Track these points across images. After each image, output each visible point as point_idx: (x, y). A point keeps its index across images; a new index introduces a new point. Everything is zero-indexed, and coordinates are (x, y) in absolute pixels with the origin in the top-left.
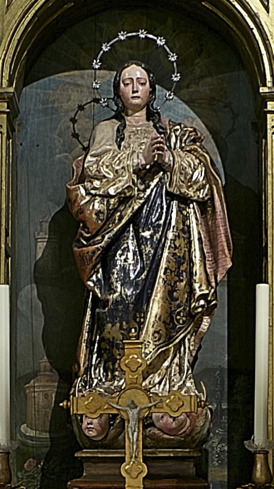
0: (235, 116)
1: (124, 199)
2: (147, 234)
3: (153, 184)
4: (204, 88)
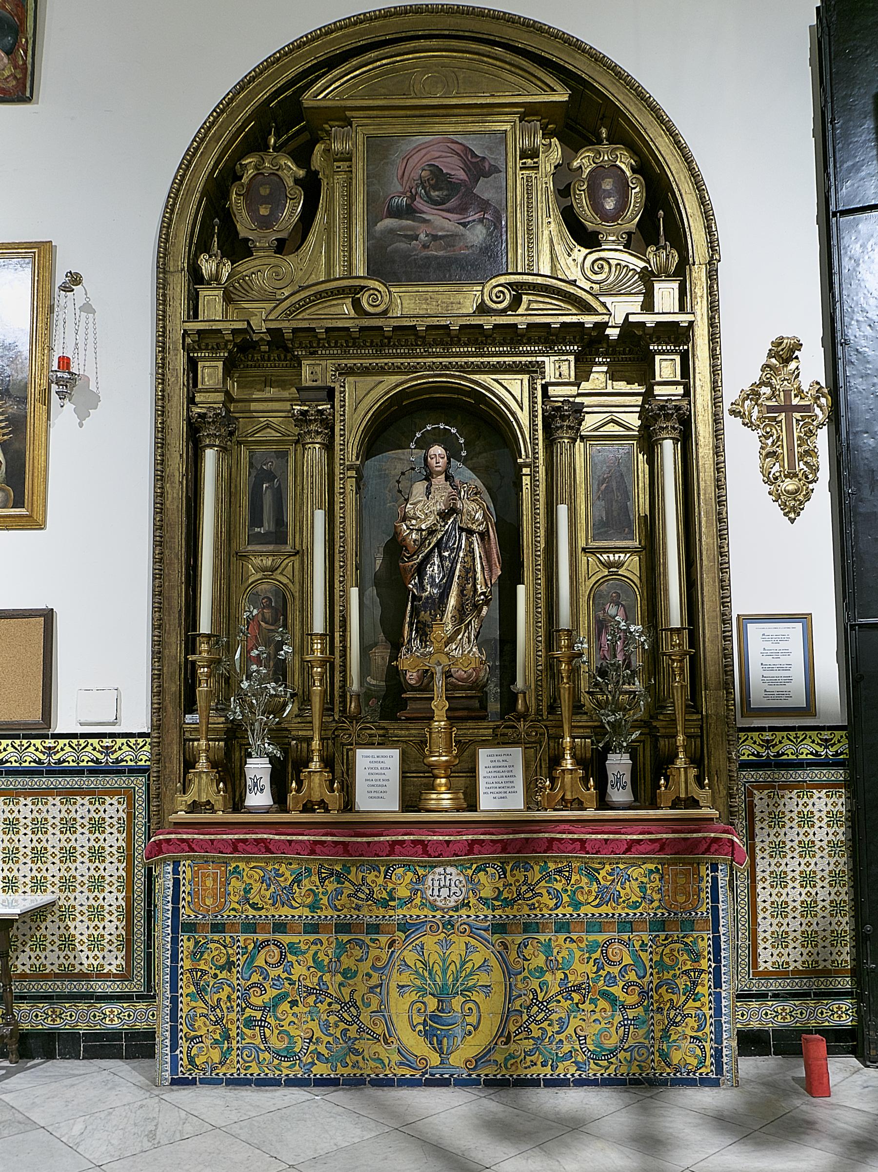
0: (502, 478)
1: (431, 532)
2: (446, 554)
3: (450, 522)
4: (482, 460)
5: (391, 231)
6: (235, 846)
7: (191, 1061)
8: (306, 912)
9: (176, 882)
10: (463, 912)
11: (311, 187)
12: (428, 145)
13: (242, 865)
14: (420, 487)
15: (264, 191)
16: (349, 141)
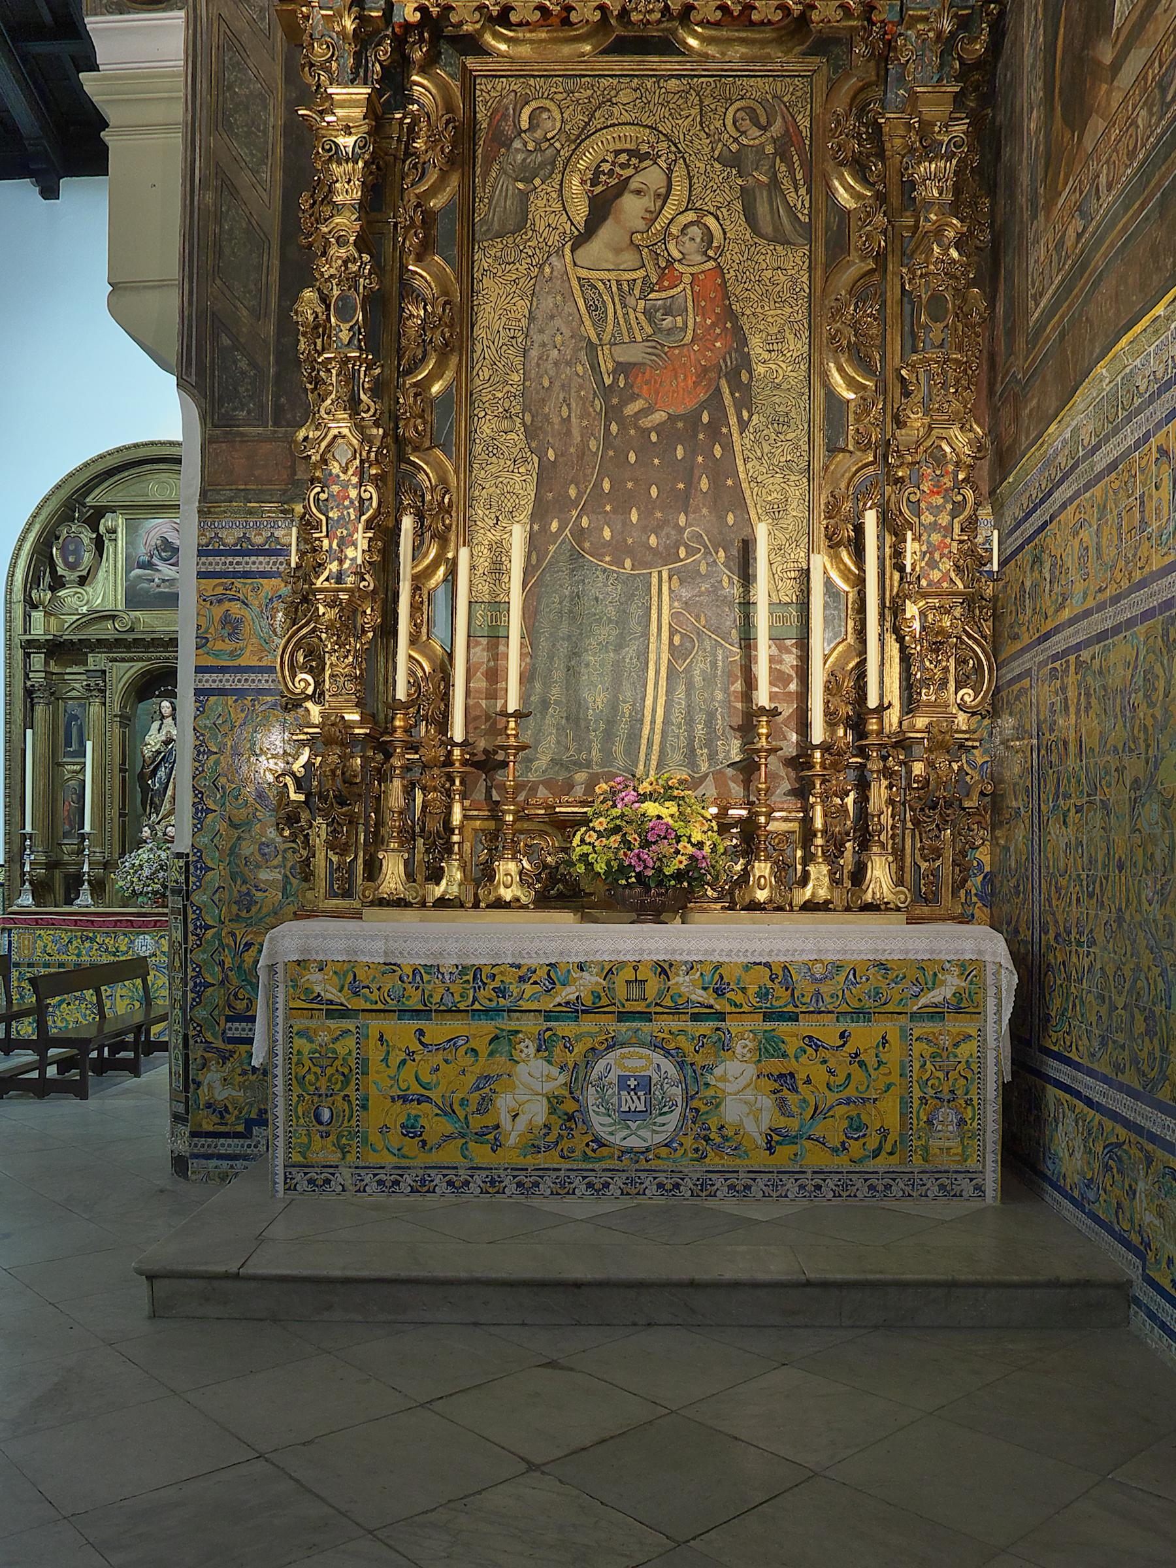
5: (139, 577)
6: (37, 921)
7: (18, 1033)
8: (75, 958)
9: (10, 942)
10: (153, 958)
11: (99, 544)
12: (161, 524)
13: (42, 932)
14: (156, 725)
15: (71, 547)
16: (116, 521)
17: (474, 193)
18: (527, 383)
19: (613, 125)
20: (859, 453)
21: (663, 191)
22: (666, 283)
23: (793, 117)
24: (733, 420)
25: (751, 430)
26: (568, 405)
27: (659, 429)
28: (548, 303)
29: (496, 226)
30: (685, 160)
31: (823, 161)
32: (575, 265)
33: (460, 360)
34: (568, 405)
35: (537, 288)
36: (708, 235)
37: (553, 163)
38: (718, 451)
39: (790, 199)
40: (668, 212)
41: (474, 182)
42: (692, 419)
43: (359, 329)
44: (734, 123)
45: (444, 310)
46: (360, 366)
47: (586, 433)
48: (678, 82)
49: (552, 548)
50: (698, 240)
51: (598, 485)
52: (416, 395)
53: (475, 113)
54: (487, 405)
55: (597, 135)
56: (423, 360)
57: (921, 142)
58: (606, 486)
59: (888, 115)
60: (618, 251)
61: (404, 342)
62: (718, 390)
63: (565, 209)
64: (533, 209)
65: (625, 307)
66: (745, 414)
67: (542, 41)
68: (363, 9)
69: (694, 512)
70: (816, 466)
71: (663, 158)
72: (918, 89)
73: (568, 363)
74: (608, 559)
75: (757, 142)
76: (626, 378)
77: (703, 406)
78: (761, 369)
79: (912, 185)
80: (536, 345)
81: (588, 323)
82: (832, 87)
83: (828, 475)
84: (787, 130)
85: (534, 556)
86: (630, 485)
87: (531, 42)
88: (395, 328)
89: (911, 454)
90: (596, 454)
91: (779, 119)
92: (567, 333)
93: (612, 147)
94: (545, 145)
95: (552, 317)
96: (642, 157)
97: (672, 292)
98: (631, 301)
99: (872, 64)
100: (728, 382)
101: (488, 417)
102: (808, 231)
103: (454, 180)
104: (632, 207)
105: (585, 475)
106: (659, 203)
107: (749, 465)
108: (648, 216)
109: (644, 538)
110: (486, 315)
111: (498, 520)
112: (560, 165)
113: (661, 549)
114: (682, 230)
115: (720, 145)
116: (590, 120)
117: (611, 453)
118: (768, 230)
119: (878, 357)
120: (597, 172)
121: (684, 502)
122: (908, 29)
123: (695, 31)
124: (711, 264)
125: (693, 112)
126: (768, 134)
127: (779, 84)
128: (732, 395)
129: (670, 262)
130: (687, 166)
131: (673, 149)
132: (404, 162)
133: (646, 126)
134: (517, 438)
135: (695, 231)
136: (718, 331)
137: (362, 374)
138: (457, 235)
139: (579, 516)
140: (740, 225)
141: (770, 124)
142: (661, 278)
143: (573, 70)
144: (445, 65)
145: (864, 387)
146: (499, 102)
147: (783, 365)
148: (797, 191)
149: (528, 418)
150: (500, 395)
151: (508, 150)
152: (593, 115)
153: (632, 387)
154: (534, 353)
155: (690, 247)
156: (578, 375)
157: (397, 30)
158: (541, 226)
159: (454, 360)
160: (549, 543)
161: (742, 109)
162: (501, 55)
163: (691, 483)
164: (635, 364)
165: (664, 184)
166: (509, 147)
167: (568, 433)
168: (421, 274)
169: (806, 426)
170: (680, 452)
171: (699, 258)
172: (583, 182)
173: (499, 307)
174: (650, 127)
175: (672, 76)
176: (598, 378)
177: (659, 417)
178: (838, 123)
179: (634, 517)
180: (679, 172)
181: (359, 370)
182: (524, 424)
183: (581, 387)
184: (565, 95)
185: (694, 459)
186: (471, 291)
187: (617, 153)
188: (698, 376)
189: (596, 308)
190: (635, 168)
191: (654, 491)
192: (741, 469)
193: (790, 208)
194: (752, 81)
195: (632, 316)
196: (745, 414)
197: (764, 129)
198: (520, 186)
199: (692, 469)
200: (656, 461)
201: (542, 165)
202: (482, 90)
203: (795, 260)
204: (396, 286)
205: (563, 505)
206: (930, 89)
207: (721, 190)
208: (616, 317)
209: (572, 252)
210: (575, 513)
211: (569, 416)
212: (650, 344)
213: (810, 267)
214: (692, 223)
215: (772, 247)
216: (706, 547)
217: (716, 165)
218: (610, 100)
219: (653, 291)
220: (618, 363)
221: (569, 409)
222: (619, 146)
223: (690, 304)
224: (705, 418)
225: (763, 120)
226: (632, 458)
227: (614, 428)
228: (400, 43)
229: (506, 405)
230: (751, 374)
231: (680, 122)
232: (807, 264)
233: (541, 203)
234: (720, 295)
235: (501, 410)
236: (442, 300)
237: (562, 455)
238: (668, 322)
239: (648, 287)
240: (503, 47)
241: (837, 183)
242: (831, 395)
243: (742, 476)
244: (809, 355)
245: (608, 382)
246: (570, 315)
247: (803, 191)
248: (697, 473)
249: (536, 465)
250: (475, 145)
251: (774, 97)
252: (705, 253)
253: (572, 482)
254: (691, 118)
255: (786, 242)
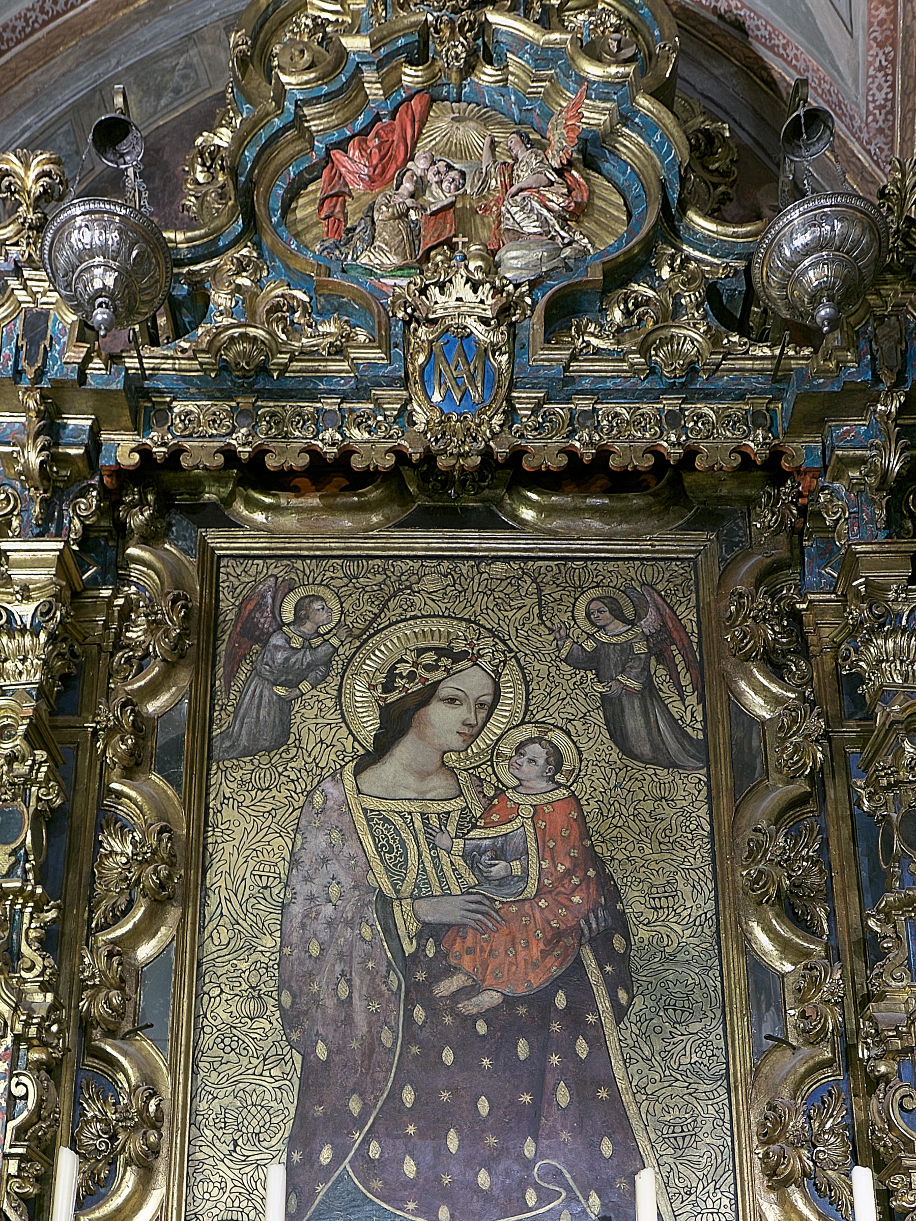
17: (212, 699)
18: (287, 950)
19: (414, 617)
20: (806, 1050)
21: (488, 699)
22: (495, 817)
23: (671, 608)
24: (604, 1004)
25: (633, 1019)
26: (349, 981)
27: (489, 1015)
28: (318, 842)
29: (244, 741)
30: (518, 661)
31: (720, 658)
32: (359, 792)
33: (184, 915)
34: (349, 981)
35: (303, 822)
36: (556, 758)
37: (328, 663)
38: (582, 1048)
39: (673, 711)
40: (496, 726)
41: (213, 685)
42: (541, 1001)
43: (26, 853)
44: (588, 615)
45: (160, 840)
46: (24, 906)
47: (376, 1021)
48: (505, 566)
49: (322, 1189)
50: (541, 762)
51: (395, 1095)
52: (110, 955)
53: (218, 600)
54: (223, 979)
55: (392, 629)
56: (124, 913)
57: (871, 611)
58: (408, 1096)
59: (811, 597)
60: (423, 775)
61: (99, 889)
62: (579, 964)
63: (344, 721)
64: (298, 720)
65: (435, 847)
66: (622, 996)
67: (313, 509)
68: (57, 445)
69: (549, 1137)
70: (740, 1069)
71: (487, 659)
72: (859, 548)
73: (349, 923)
74: (411, 1206)
75: (621, 639)
76: (438, 944)
77: (556, 984)
78: (643, 933)
79: (858, 679)
80: (300, 898)
81: (378, 868)
82: (727, 569)
83: (762, 1081)
84: (665, 624)
85: (293, 1201)
86: (445, 1096)
87: (299, 510)
88: (86, 869)
89: (899, 1035)
90: (391, 1051)
91: (652, 612)
92: (347, 882)
93: (412, 645)
94: (317, 642)
95: (325, 861)
96: (457, 658)
97: (504, 829)
98: (443, 840)
99: (782, 537)
100: (595, 951)
101: (224, 996)
102: (703, 752)
103: (184, 678)
104: (443, 721)
105: (374, 1081)
106: (482, 714)
107: (633, 1069)
108: (466, 730)
109: (469, 1175)
110: (226, 856)
111: (236, 1145)
112: (337, 665)
113: (496, 1192)
114: (517, 750)
115: (568, 642)
116: (382, 611)
117: (415, 1050)
118: (646, 750)
119: (823, 914)
120: (392, 675)
121: (531, 1122)
122: (835, 479)
123: (529, 499)
124: (562, 793)
125: (528, 602)
126: (637, 629)
127: (649, 569)
128: (601, 968)
129: (500, 792)
130: (522, 669)
131: (501, 646)
132: (112, 655)
133: (462, 619)
134: (268, 1026)
135: (535, 750)
136: (576, 881)
137: (26, 920)
138: (188, 756)
139: (366, 1142)
140: (603, 743)
141: (639, 617)
142: (488, 809)
143: (357, 549)
144: (177, 539)
145: (808, 954)
146: (253, 589)
147: (678, 928)
148: (683, 700)
149: (286, 999)
150: (244, 966)
151: (263, 647)
152: (386, 605)
153: (446, 956)
154: (297, 909)
155: (528, 771)
156: (363, 939)
157: (106, 479)
158: (309, 742)
159: (173, 914)
160: (317, 1181)
161: (598, 599)
162: (256, 527)
163: (542, 1094)
164: (450, 926)
165: (489, 689)
166: (265, 643)
167: (349, 1021)
168: (132, 796)
169: (719, 1013)
170: (523, 1049)
171: (543, 785)
172: (372, 687)
173: (247, 843)
174: (469, 621)
175: (497, 559)
176: (395, 943)
177: (489, 999)
178: (740, 606)
179: (453, 1143)
180: (510, 675)
181: (22, 912)
182: (280, 1007)
183: (368, 957)
184: (346, 580)
185: (545, 1059)
186: (203, 821)
187: (421, 652)
188: (548, 942)
189: (392, 851)
190: (447, 670)
191: (484, 1106)
192: (619, 1072)
193: (672, 721)
194: (611, 566)
195: (445, 860)
196: (622, 996)
197: (632, 623)
198: (281, 691)
199: (543, 1073)
200: (486, 1062)
201: (311, 667)
202: (228, 574)
203: (688, 788)
204: (92, 813)
205: (340, 1126)
206: (875, 547)
207: (574, 704)
208: (421, 861)
209: (355, 775)
210: (358, 1137)
211: (350, 997)
212: (472, 898)
213: (709, 797)
214: (531, 740)
215: (651, 772)
216: (569, 1190)
217: (564, 667)
218: (410, 588)
219: (475, 826)
220: (425, 924)
221: (350, 986)
222: (422, 645)
223: (532, 845)
224: (561, 1001)
225: (629, 612)
226: (448, 1056)
227: (419, 1013)
228: (111, 499)
229: (254, 981)
230: (628, 940)
231: (510, 614)
232: (704, 793)
233: (310, 714)
234: (576, 833)
235: (245, 986)
236: (157, 827)
237: (339, 1051)
238: (499, 869)
239: (467, 822)
240: (259, 517)
241: (743, 685)
242: (757, 968)
243: (622, 1085)
244: (717, 914)
245: (409, 948)
246: (352, 857)
247: (692, 700)
248: (550, 1079)
249: (298, 1066)
250: (216, 639)
251: (643, 584)
252: (552, 779)
253: (353, 1091)
254: (525, 609)
255: (672, 765)
